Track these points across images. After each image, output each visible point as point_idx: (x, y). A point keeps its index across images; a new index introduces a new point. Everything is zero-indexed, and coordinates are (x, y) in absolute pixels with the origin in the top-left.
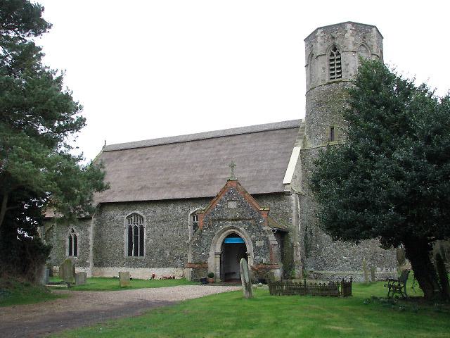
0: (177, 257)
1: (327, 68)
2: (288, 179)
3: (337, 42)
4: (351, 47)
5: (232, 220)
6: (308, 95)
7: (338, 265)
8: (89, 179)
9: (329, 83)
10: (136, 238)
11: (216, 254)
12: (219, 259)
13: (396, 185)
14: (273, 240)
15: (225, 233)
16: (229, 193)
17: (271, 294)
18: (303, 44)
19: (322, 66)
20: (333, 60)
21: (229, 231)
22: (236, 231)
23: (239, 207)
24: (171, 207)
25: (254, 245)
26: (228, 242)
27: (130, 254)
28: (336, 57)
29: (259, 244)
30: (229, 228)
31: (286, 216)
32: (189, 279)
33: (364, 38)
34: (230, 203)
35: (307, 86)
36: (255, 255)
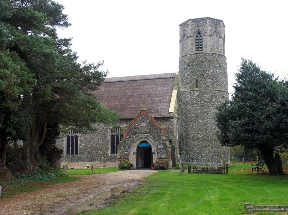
0: (101, 155)
1: (194, 44)
2: (172, 109)
3: (200, 29)
4: (209, 33)
5: (144, 133)
6: (181, 59)
10: (72, 143)
11: (134, 153)
12: (135, 156)
13: (269, 123)
14: (168, 143)
15: (139, 141)
16: (142, 118)
17: (189, 173)
18: (179, 28)
19: (190, 44)
20: (198, 40)
21: (142, 139)
22: (146, 140)
23: (148, 125)
25: (157, 148)
26: (140, 146)
27: (68, 153)
28: (199, 38)
31: (170, 131)
32: (118, 167)
33: (216, 27)
34: (142, 123)
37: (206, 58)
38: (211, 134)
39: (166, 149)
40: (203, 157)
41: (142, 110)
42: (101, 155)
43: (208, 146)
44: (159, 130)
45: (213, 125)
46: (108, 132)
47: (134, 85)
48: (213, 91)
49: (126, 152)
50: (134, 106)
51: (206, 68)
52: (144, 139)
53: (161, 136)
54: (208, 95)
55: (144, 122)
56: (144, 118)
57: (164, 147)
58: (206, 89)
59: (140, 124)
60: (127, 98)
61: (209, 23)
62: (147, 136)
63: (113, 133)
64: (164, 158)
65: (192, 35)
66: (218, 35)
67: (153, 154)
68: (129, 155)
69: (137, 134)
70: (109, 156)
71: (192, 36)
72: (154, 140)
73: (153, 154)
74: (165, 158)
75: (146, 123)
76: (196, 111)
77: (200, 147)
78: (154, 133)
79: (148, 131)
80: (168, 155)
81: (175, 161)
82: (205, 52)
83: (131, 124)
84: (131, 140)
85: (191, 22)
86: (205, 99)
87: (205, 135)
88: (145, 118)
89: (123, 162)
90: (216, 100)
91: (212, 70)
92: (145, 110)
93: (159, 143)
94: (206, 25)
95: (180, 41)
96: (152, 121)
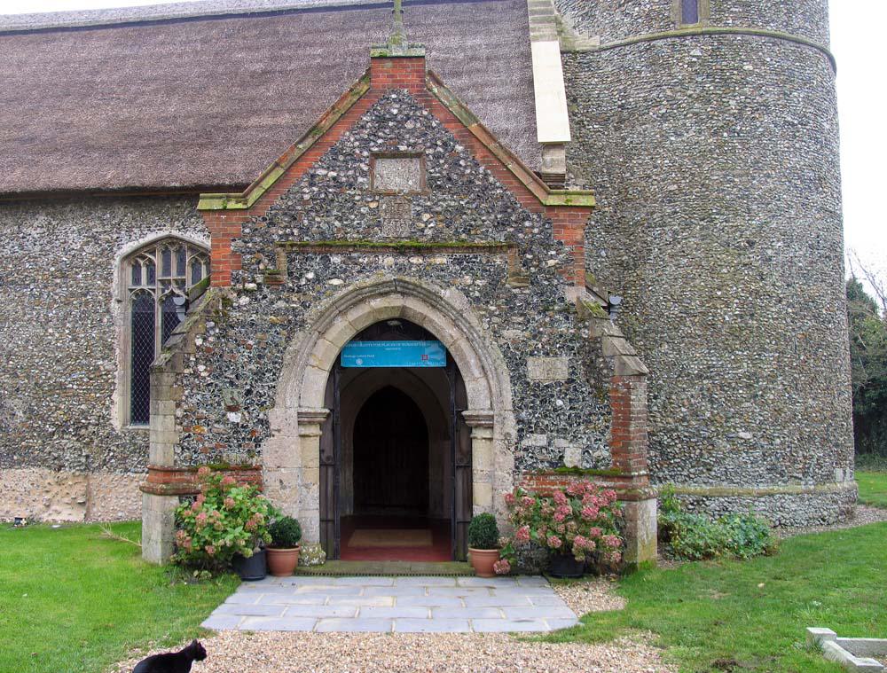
0: (62, 428)
5: (401, 250)
11: (304, 419)
12: (314, 444)
15: (354, 314)
16: (381, 121)
21: (377, 303)
22: (416, 307)
23: (431, 184)
24: (35, 227)
25: (519, 378)
26: (359, 363)
29: (547, 369)
30: (381, 290)
36: (525, 428)
39: (599, 392)
40: (739, 446)
41: (382, 58)
42: (62, 428)
43: (772, 378)
44: (533, 227)
46: (108, 280)
47: (280, 28)
48: (790, 46)
49: (231, 409)
50: (285, 119)
52: (396, 301)
53: (552, 273)
55: (397, 155)
56: (401, 124)
57: (581, 370)
59: (364, 174)
60: (243, 85)
62: (422, 273)
63: (144, 285)
64: (576, 471)
67: (478, 433)
68: (258, 442)
69: (336, 259)
70: (117, 437)
72: (492, 314)
73: (478, 433)
74: (594, 472)
75: (415, 165)
76: (692, 158)
77: (722, 386)
78: (491, 249)
79: (438, 232)
80: (620, 446)
83: (281, 171)
84: (281, 304)
87: (754, 306)
88: (409, 125)
89: (207, 513)
92: (410, 58)
93: (536, 335)
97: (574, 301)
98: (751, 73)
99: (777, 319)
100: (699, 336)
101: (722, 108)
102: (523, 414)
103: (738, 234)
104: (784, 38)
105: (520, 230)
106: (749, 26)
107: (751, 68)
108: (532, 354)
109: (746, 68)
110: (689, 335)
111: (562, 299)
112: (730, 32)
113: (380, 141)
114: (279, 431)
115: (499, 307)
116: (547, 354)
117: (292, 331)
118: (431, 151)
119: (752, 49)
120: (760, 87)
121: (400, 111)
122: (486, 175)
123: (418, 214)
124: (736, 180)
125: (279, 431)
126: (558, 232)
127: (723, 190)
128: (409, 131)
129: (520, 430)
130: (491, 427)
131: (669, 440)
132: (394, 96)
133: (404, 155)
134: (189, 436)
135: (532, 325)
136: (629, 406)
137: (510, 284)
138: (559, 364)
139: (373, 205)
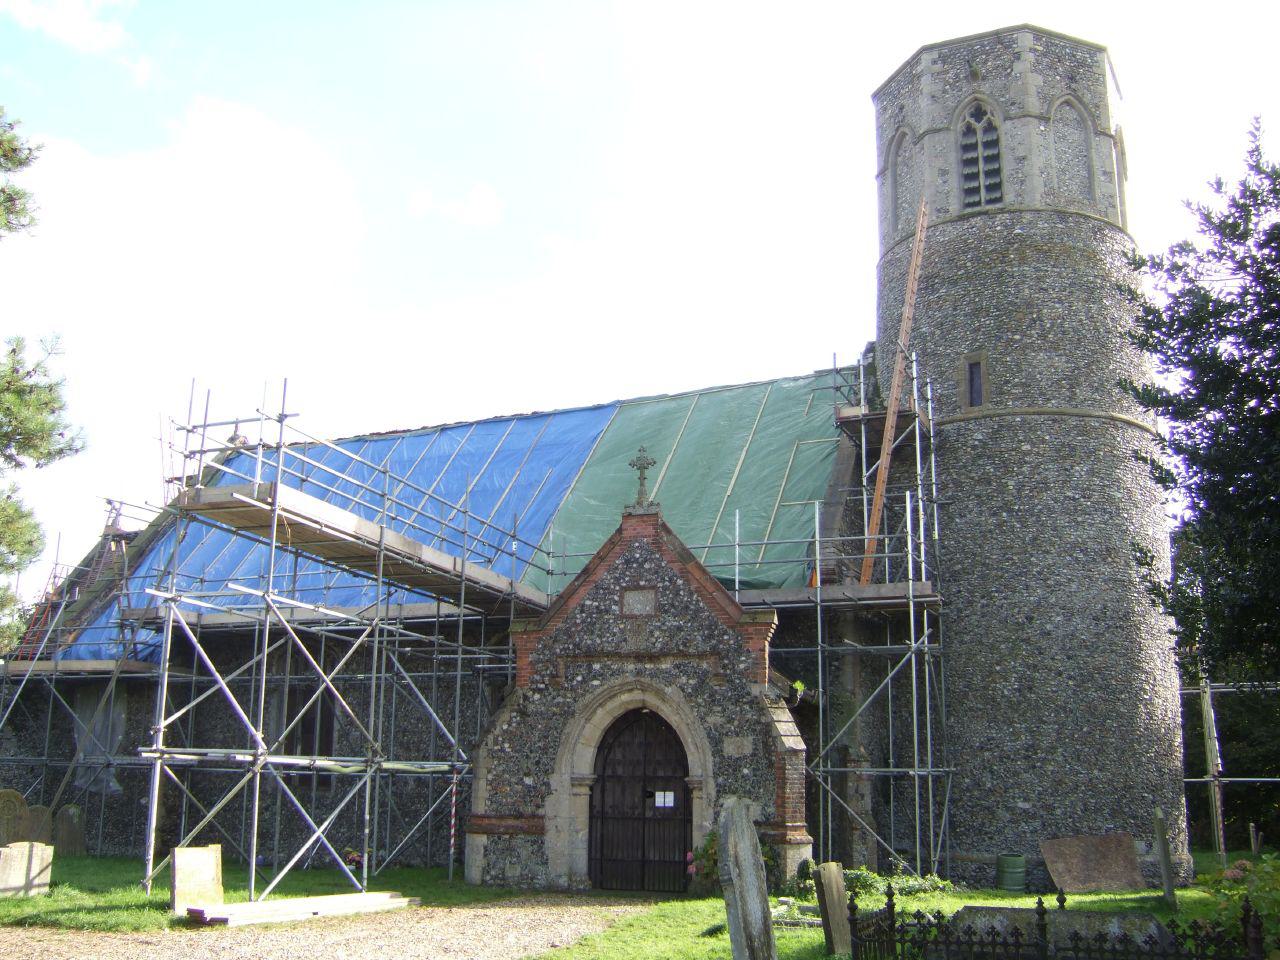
5: (639, 657)
7: (1000, 832)
8: (1049, 634)
9: (962, 218)
11: (576, 782)
12: (584, 801)
15: (610, 705)
16: (627, 562)
18: (870, 111)
21: (625, 697)
23: (661, 609)
29: (738, 746)
33: (1072, 79)
35: (884, 237)
37: (1021, 239)
38: (1070, 678)
43: (1052, 749)
45: (1077, 620)
48: (1073, 422)
49: (527, 775)
51: (1027, 291)
52: (637, 695)
54: (1043, 441)
56: (641, 565)
58: (1031, 410)
59: (616, 603)
61: (1031, 57)
65: (942, 126)
66: (1083, 120)
68: (543, 798)
69: (597, 666)
71: (939, 130)
75: (651, 595)
81: (851, 842)
82: (1017, 207)
84: (560, 699)
85: (935, 62)
86: (1025, 469)
87: (1032, 679)
88: (647, 566)
90: (1091, 472)
91: (1060, 301)
94: (1018, 67)
95: (881, 174)
96: (687, 582)
97: (758, 694)
98: (1026, 454)
99: (1056, 692)
100: (980, 710)
101: (1002, 489)
102: (720, 780)
103: (1016, 610)
104: (1068, 414)
105: (720, 642)
106: (1029, 406)
107: (1029, 447)
108: (727, 735)
109: (1024, 448)
110: (971, 709)
111: (749, 694)
112: (1009, 414)
113: (627, 579)
114: (556, 790)
115: (704, 700)
116: (737, 735)
117: (566, 718)
118: (660, 585)
119: (1030, 429)
120: (1038, 466)
121: (641, 555)
122: (698, 601)
123: (651, 632)
124: (1015, 558)
125: (556, 790)
126: (747, 642)
127: (1002, 569)
128: (647, 571)
129: (718, 792)
130: (701, 789)
131: (955, 810)
132: (637, 544)
133: (643, 588)
134: (496, 793)
135: (727, 713)
136: (784, 773)
137: (713, 683)
138: (745, 742)
139: (622, 626)
